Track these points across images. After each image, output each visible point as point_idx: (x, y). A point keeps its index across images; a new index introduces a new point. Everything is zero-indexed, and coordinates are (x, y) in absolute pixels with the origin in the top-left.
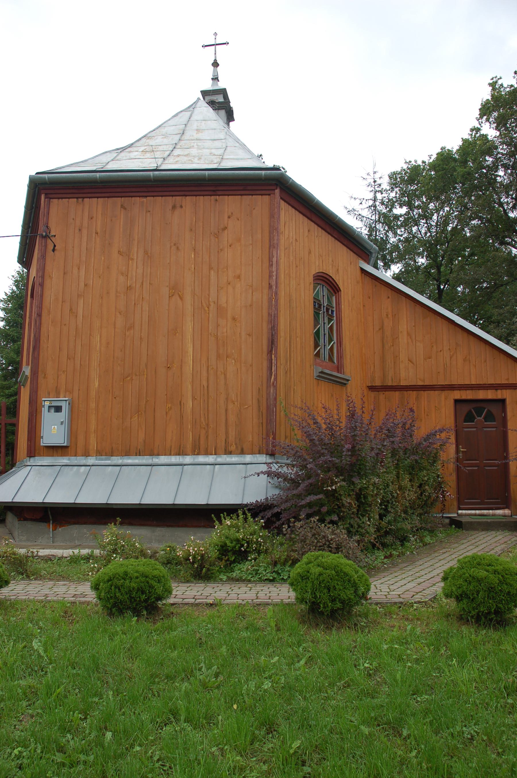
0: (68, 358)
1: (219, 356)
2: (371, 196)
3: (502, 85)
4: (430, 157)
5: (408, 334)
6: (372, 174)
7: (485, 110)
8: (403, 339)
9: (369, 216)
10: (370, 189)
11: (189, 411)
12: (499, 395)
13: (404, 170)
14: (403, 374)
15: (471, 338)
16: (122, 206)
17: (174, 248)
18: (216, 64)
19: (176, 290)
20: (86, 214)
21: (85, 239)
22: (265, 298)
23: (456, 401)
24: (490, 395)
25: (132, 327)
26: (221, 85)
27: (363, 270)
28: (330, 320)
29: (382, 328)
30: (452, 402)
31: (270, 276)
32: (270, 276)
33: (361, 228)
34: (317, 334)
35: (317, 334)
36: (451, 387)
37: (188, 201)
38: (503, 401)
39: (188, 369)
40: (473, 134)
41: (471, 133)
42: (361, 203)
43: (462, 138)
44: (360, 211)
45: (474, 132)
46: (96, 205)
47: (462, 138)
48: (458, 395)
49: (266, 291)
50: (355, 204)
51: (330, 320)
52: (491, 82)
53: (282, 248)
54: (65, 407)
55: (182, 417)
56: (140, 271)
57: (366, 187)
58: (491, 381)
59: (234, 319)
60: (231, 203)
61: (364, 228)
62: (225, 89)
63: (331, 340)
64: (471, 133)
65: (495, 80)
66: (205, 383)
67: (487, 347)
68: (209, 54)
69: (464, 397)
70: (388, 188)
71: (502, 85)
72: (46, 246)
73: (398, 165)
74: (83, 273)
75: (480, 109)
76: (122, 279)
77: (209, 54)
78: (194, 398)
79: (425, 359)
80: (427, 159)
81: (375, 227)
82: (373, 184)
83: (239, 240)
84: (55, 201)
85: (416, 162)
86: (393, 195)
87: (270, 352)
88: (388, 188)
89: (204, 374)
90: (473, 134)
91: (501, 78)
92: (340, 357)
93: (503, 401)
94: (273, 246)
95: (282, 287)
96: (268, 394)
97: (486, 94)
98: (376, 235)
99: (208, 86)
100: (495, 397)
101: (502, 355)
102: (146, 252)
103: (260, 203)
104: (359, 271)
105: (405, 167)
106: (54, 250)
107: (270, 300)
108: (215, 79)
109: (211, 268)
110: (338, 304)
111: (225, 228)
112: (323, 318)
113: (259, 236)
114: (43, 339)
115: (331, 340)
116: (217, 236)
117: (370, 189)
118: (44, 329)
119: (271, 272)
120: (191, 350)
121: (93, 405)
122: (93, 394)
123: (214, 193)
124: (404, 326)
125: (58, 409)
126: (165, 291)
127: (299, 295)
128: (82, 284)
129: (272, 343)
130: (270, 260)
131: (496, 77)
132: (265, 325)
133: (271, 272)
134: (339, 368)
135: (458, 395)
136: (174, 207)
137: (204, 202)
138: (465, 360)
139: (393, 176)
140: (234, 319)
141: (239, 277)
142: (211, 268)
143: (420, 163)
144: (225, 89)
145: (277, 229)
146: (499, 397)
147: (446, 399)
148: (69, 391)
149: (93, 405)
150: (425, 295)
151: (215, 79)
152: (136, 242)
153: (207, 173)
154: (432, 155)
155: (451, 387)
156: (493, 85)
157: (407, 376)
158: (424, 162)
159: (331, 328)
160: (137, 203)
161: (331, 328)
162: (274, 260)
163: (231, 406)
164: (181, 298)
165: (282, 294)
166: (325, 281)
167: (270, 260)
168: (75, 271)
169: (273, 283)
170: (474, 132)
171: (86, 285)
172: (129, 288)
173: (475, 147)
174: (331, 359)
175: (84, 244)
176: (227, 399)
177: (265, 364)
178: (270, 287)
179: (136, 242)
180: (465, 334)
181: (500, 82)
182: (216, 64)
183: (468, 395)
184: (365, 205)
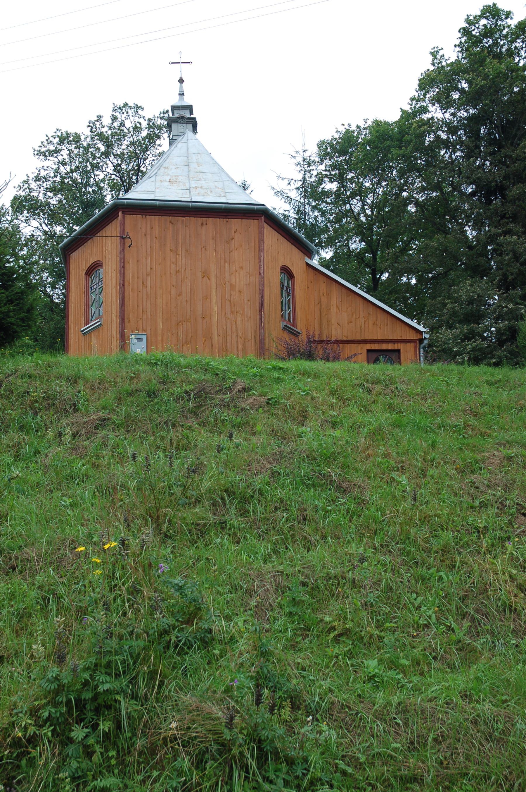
0: (143, 311)
1: (232, 312)
2: (300, 176)
3: (443, 56)
4: (366, 121)
5: (337, 307)
6: (301, 153)
7: (426, 83)
8: (334, 310)
9: (298, 199)
10: (299, 168)
11: (216, 342)
12: (396, 346)
13: (336, 139)
14: (334, 333)
15: (378, 310)
16: (170, 222)
17: (203, 249)
18: (181, 81)
19: (206, 274)
20: (149, 225)
21: (149, 241)
22: (257, 280)
23: (368, 351)
24: (390, 347)
25: (180, 294)
26: (187, 101)
27: (307, 264)
28: (289, 295)
29: (320, 303)
30: (365, 351)
31: (260, 268)
32: (260, 268)
33: (289, 211)
34: (282, 302)
35: (282, 302)
36: (365, 342)
37: (210, 221)
38: (398, 351)
39: (215, 319)
40: (414, 105)
41: (410, 103)
42: (289, 184)
43: (401, 109)
44: (288, 192)
45: (414, 102)
46: (155, 220)
47: (401, 109)
48: (369, 346)
49: (257, 276)
50: (282, 185)
51: (289, 295)
52: (432, 51)
53: (265, 251)
54: (144, 338)
55: (212, 345)
56: (184, 261)
57: (294, 166)
58: (391, 338)
59: (240, 291)
60: (236, 224)
61: (292, 211)
62: (192, 106)
63: (289, 308)
64: (410, 103)
65: (436, 49)
66: (225, 327)
67: (389, 316)
68: (176, 72)
69: (373, 348)
70: (317, 159)
71: (443, 56)
72: (124, 244)
73: (330, 133)
74: (149, 261)
75: (420, 80)
76: (173, 266)
77: (176, 72)
78: (219, 335)
79: (348, 323)
80: (362, 124)
81: (304, 210)
82: (302, 163)
83: (241, 246)
84: (128, 216)
85: (350, 125)
86: (322, 167)
87: (261, 310)
88: (317, 159)
89: (224, 321)
90: (414, 105)
91: (442, 49)
92: (294, 319)
93: (398, 351)
94: (261, 250)
95: (265, 273)
96: (260, 333)
97: (426, 65)
98: (305, 219)
99: (176, 101)
100: (393, 348)
101: (398, 321)
102: (187, 251)
103: (253, 224)
104: (305, 265)
105: (337, 136)
106: (129, 247)
107: (260, 281)
108: (182, 94)
109: (225, 262)
110: (293, 285)
111: (233, 238)
112: (285, 294)
113: (253, 244)
114: (126, 299)
115: (289, 308)
116: (228, 242)
117: (299, 168)
118: (126, 294)
119: (260, 266)
120: (216, 308)
121: (160, 338)
122: (159, 332)
123: (226, 217)
124: (334, 301)
125: (140, 339)
126: (200, 275)
127: (274, 278)
128: (149, 268)
129: (262, 305)
130: (259, 258)
131: (437, 47)
132: (257, 295)
133: (260, 266)
134: (294, 325)
135: (369, 346)
136: (202, 224)
137: (220, 222)
138: (374, 324)
139: (322, 145)
140: (240, 291)
141: (242, 267)
142: (225, 262)
143: (353, 127)
144: (192, 106)
145: (263, 240)
146: (396, 348)
147: (361, 349)
148: (144, 330)
149: (160, 338)
150: (359, 286)
151: (182, 94)
152: (180, 244)
153: (223, 205)
154: (367, 119)
155: (365, 342)
156: (434, 54)
157: (336, 333)
158: (358, 127)
159: (289, 300)
160: (179, 220)
161: (289, 300)
162: (262, 258)
163: (239, 339)
164: (209, 279)
165: (266, 278)
166: (286, 271)
167: (259, 258)
168: (144, 260)
169: (262, 272)
170: (414, 102)
171: (151, 269)
172: (178, 272)
173: (411, 126)
174: (289, 320)
175: (148, 244)
176: (237, 335)
177: (258, 317)
178: (260, 274)
179: (180, 244)
180: (374, 307)
181: (441, 53)
182: (181, 81)
183: (376, 347)
184: (293, 186)
